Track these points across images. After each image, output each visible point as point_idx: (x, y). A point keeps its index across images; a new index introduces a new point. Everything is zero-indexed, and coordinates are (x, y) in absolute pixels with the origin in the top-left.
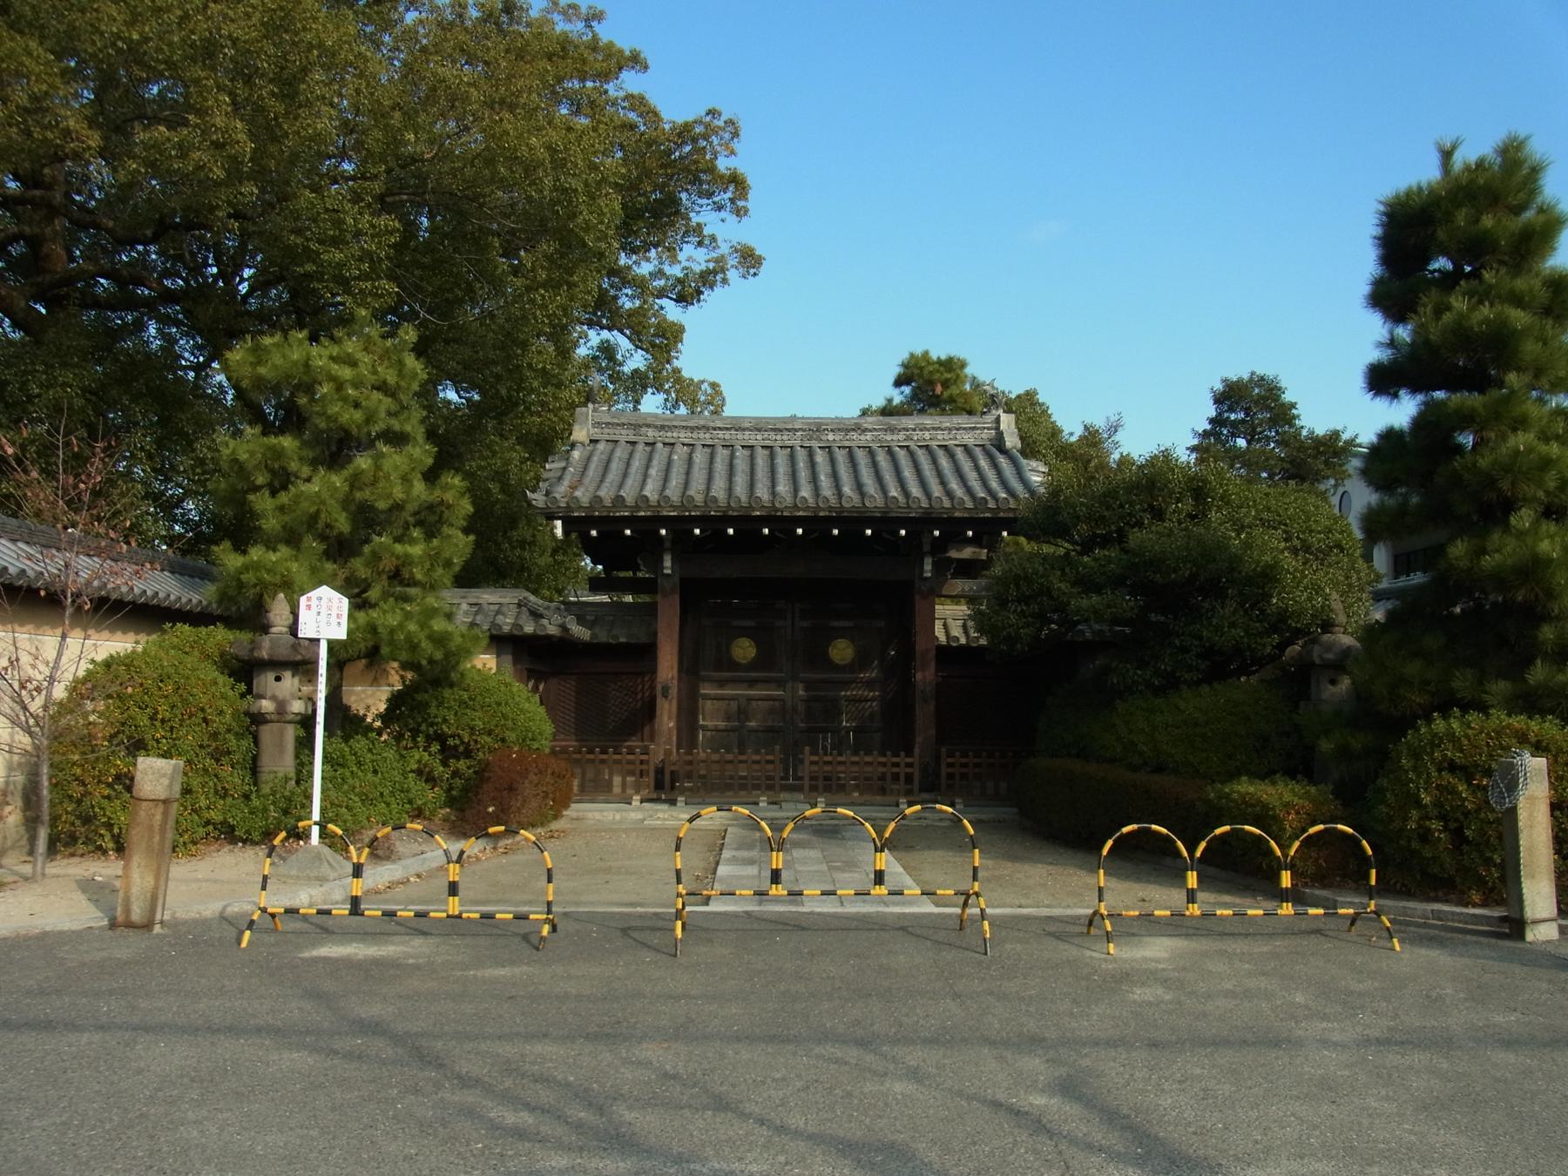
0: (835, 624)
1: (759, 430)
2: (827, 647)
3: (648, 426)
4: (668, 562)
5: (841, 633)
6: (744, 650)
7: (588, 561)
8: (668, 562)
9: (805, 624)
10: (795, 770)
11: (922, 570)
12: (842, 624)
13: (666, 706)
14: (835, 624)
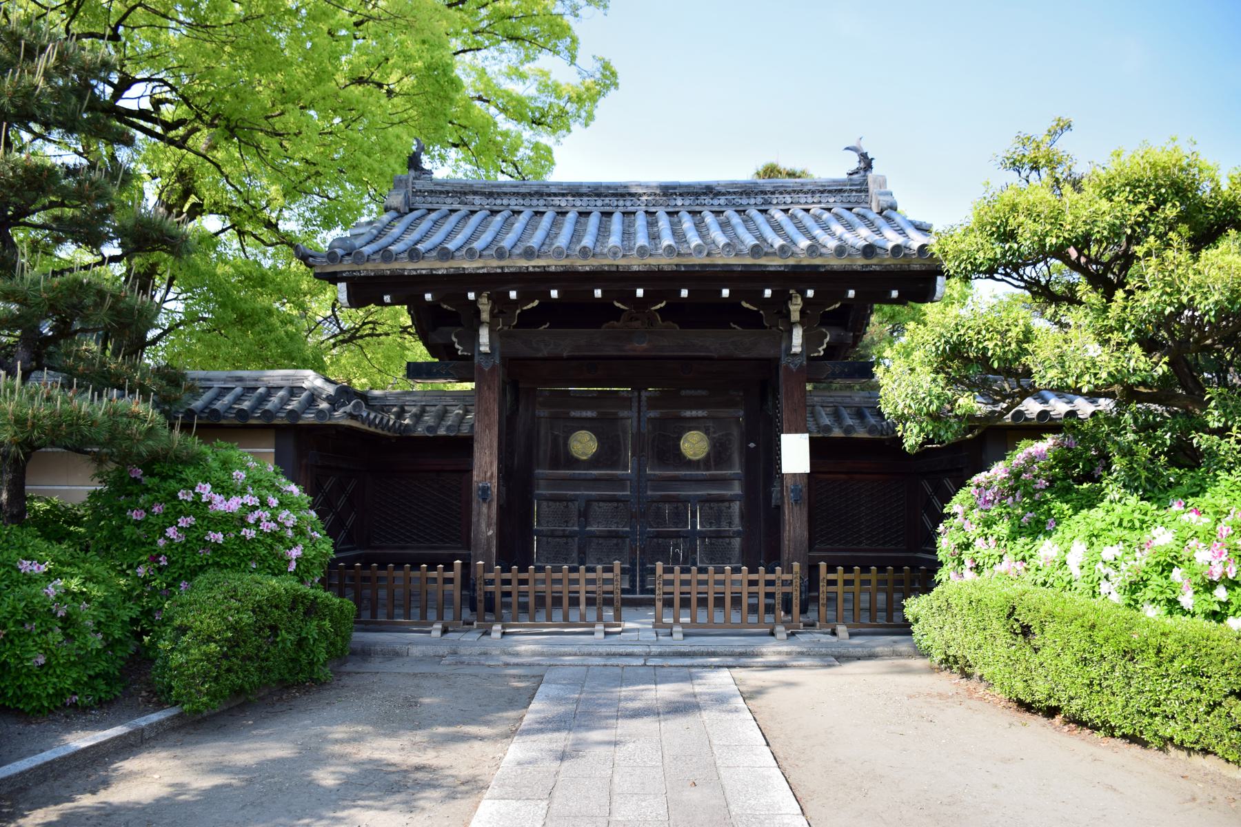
0: (688, 414)
1: (599, 195)
2: (679, 439)
3: (475, 193)
4: (484, 336)
5: (693, 424)
6: (387, 298)
7: (102, 146)
8: (484, 336)
9: (653, 414)
10: (643, 581)
11: (790, 346)
12: (694, 413)
13: (484, 509)
14: (688, 414)
